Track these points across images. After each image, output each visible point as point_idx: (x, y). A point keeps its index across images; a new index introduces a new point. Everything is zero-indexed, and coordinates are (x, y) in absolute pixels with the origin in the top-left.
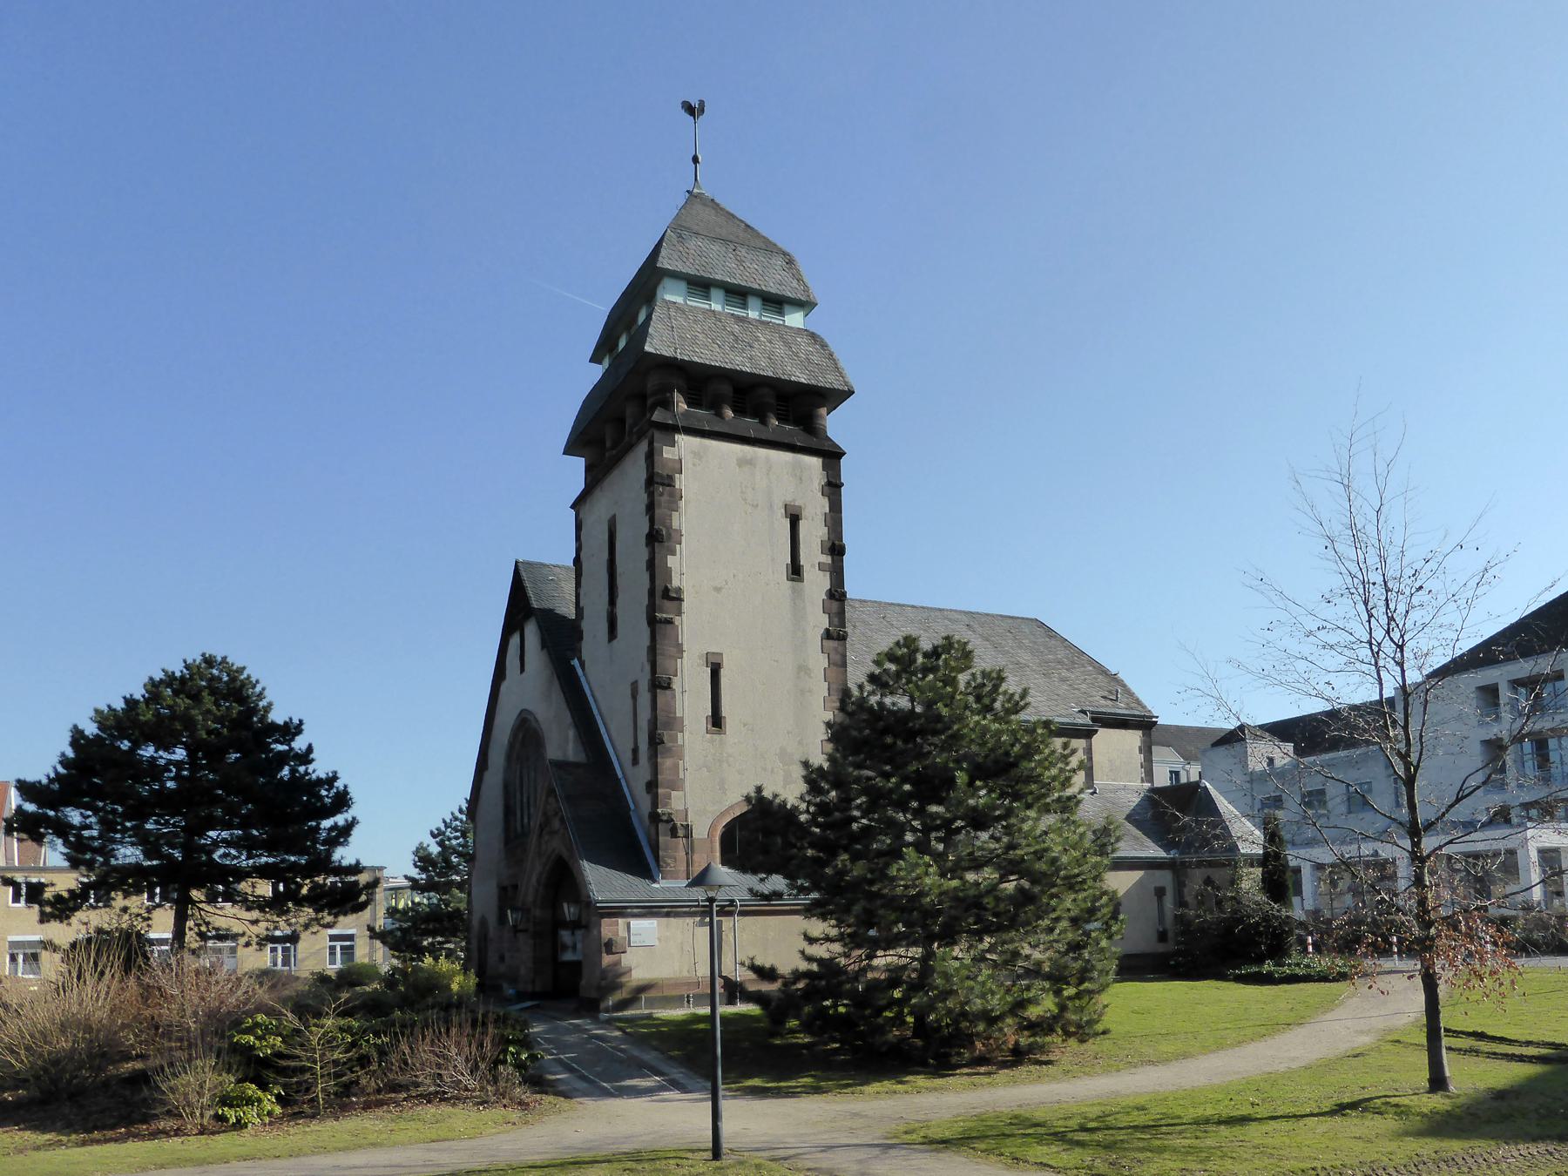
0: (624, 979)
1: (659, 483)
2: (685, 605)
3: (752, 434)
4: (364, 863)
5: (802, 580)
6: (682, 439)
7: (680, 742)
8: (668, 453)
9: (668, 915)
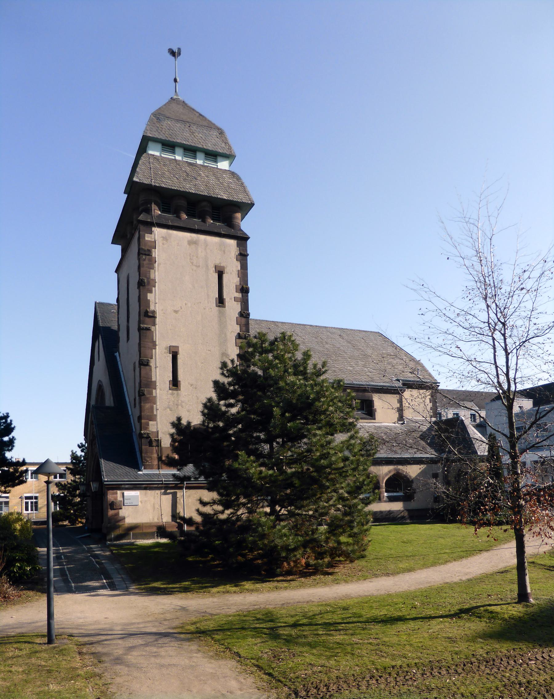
0: (120, 524)
1: (145, 254)
2: (157, 320)
3: (196, 227)
4: (27, 461)
5: (224, 307)
6: (157, 231)
7: (154, 394)
8: (148, 237)
9: (145, 489)
